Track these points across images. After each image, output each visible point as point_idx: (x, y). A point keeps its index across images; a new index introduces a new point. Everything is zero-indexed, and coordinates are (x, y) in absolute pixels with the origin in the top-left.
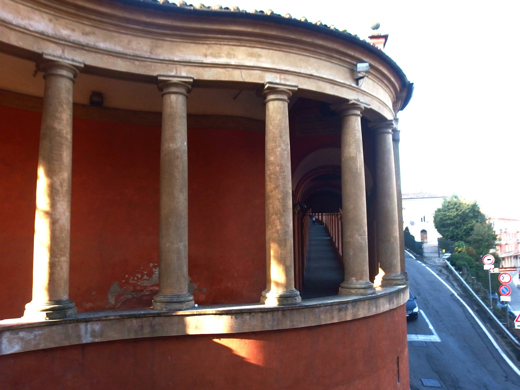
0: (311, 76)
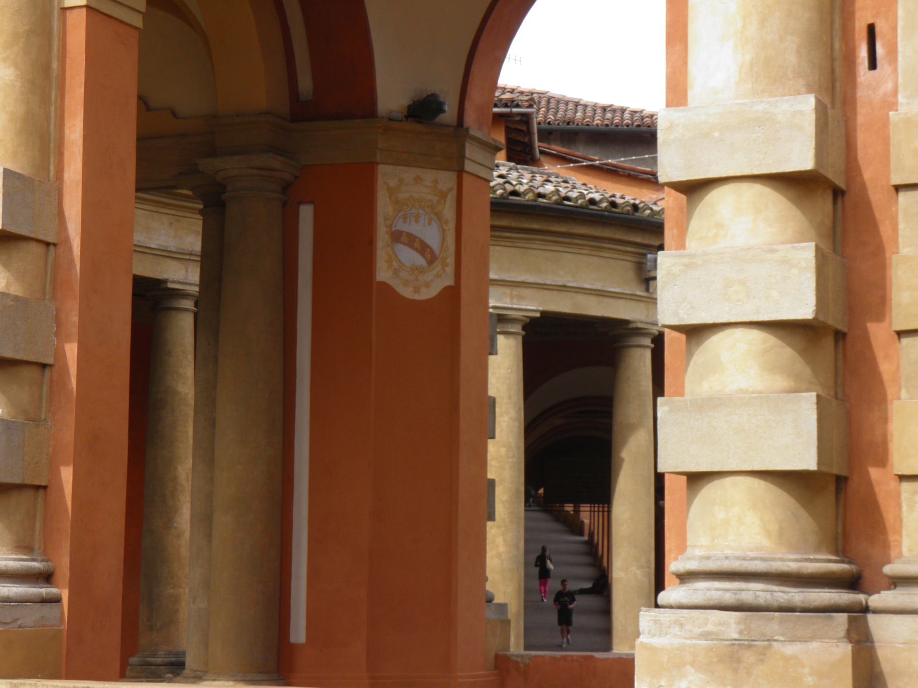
0: (563, 288)
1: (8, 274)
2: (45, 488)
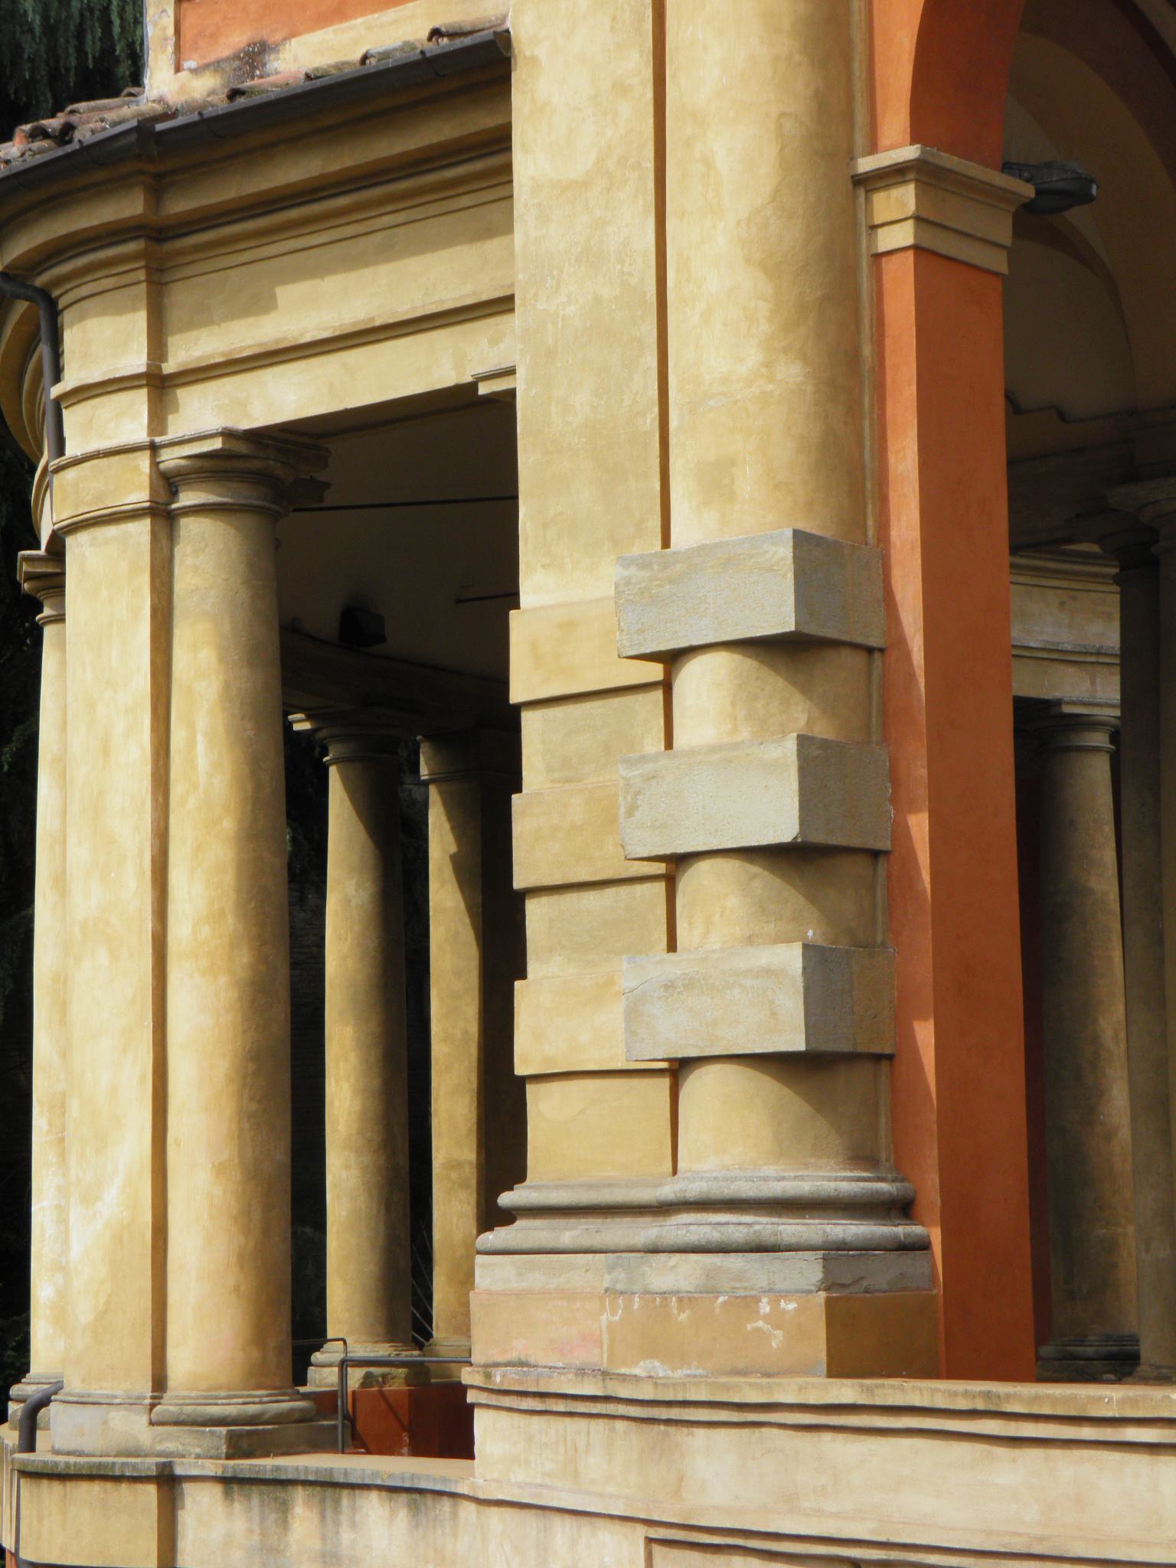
1: (809, 703)
2: (890, 1057)
